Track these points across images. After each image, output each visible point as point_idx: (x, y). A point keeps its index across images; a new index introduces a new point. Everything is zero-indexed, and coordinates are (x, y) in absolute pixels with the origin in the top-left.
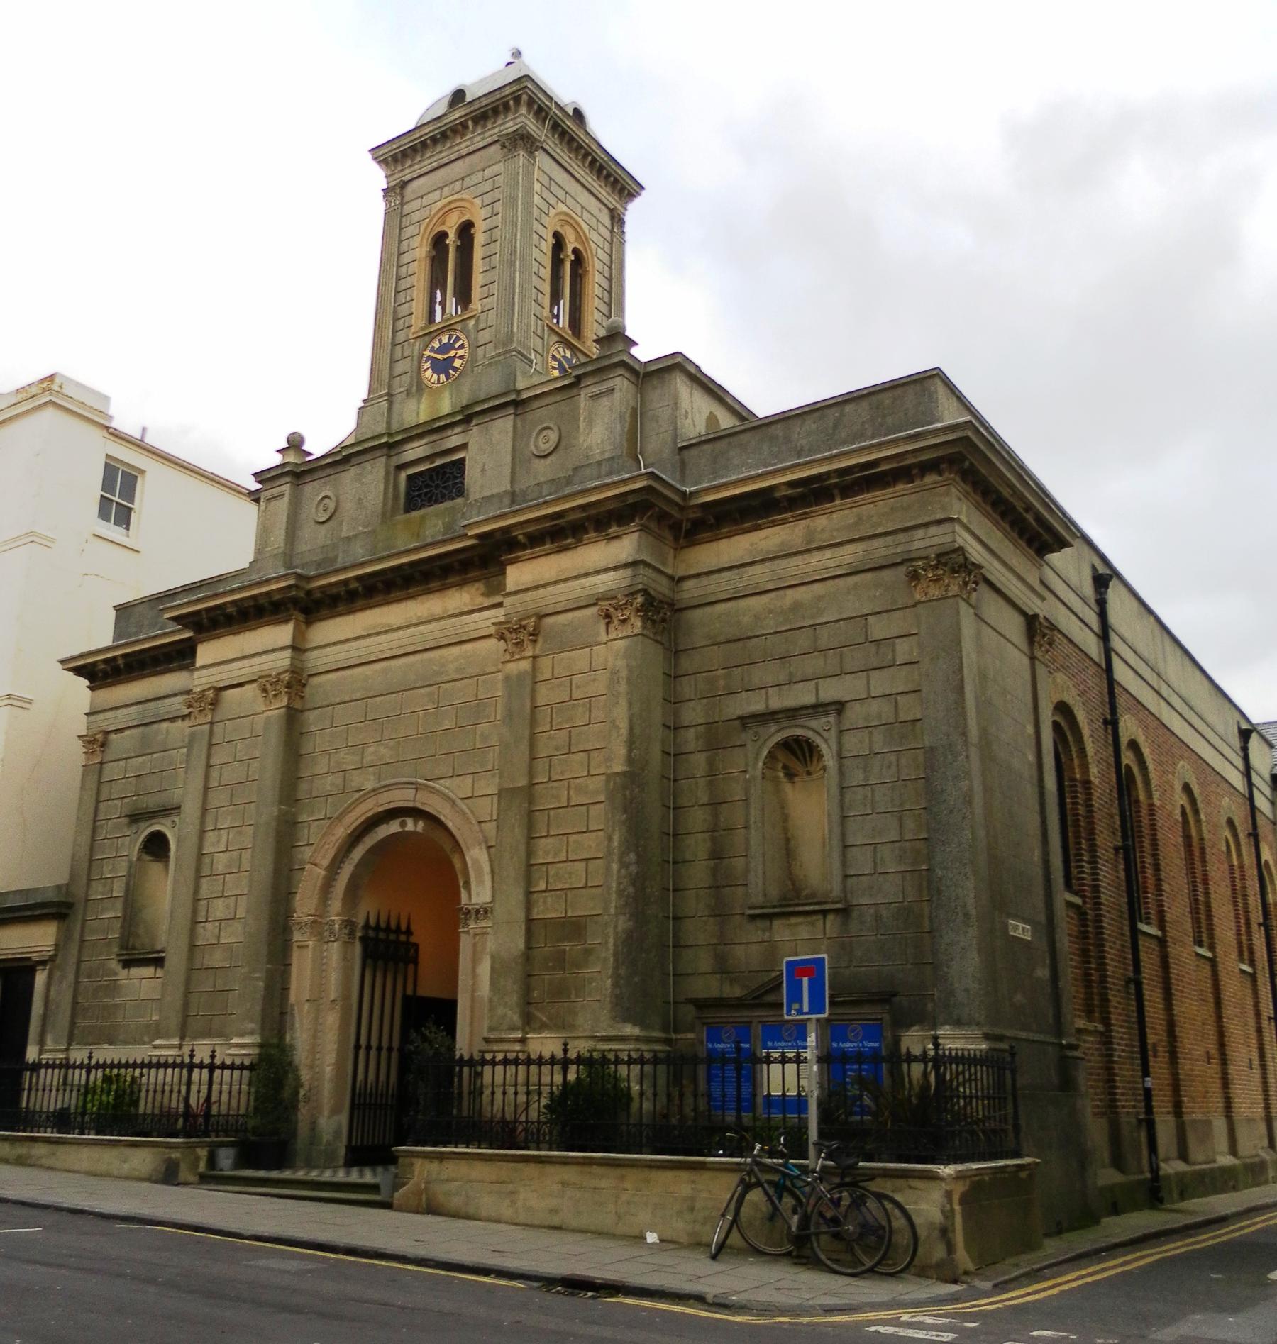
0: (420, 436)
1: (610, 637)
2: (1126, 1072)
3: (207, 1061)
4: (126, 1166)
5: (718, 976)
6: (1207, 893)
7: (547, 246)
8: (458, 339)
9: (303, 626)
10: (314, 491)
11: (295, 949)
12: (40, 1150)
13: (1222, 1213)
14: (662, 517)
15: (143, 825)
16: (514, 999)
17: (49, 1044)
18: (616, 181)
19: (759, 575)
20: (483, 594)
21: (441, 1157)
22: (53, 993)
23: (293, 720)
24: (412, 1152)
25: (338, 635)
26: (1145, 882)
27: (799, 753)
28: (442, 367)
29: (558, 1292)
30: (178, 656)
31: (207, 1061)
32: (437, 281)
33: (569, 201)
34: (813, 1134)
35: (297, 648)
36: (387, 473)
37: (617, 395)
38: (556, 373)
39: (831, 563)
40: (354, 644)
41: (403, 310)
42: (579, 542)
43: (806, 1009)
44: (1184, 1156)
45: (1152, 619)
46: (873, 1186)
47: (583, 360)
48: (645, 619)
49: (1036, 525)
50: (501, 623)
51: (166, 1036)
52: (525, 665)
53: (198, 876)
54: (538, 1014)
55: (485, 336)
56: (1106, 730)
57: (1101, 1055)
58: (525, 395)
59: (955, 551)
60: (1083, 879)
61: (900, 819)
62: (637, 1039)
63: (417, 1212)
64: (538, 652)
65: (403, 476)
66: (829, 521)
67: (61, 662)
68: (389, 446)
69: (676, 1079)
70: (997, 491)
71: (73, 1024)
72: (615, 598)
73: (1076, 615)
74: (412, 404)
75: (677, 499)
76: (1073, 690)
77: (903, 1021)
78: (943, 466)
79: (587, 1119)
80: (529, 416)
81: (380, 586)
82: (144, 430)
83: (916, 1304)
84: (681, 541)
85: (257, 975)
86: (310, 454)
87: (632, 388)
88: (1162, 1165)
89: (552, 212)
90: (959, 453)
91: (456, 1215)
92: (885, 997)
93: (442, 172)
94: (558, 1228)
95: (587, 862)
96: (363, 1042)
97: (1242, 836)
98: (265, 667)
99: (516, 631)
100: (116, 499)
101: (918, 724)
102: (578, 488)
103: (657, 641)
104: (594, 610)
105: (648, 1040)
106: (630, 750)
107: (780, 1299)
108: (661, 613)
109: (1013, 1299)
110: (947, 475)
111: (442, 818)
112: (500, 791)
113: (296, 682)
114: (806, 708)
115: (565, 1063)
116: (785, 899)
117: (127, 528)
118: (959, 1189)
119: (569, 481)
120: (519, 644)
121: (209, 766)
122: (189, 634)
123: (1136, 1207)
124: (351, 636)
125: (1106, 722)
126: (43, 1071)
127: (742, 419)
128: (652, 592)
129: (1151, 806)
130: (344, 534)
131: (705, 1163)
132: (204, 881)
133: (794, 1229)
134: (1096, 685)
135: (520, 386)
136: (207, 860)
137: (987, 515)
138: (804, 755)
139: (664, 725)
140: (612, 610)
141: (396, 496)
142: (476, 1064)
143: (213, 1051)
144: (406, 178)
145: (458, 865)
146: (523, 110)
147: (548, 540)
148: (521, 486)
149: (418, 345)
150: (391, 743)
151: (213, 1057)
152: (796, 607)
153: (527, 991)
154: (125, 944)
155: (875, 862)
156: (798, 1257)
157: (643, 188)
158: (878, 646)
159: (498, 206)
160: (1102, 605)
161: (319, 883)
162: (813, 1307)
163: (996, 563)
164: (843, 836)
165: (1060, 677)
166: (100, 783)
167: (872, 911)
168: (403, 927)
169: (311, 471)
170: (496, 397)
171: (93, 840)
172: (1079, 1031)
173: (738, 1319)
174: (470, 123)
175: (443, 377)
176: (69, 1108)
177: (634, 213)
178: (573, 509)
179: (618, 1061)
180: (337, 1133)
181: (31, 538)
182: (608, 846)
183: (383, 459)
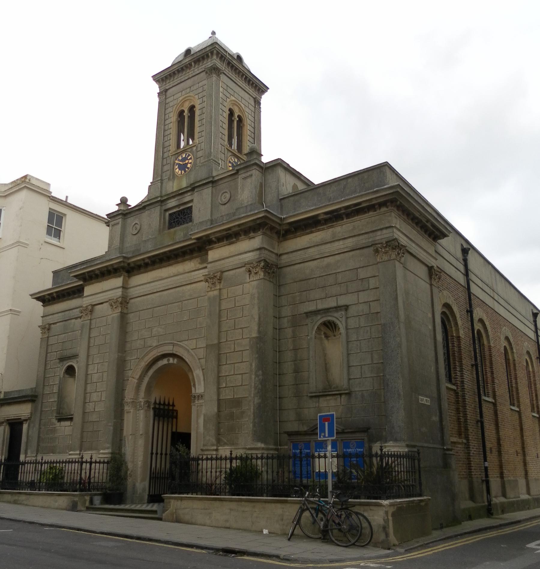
0: (174, 197)
1: (251, 280)
2: (476, 459)
3: (89, 460)
4: (57, 504)
5: (297, 422)
6: (516, 383)
7: (226, 114)
8: (189, 155)
9: (127, 278)
10: (131, 221)
11: (125, 413)
12: (23, 497)
13: (519, 519)
14: (272, 229)
15: (65, 362)
17: (29, 454)
18: (256, 86)
19: (313, 252)
20: (199, 263)
21: (182, 499)
22: (30, 433)
23: (123, 317)
24: (170, 497)
25: (142, 281)
26: (487, 379)
27: (330, 327)
28: (183, 167)
29: (220, 555)
30: (78, 292)
31: (89, 460)
32: (180, 131)
33: (236, 95)
34: (330, 488)
35: (125, 287)
36: (161, 213)
37: (254, 178)
38: (231, 168)
39: (342, 246)
40: (148, 285)
41: (167, 144)
42: (238, 240)
43: (327, 435)
44: (504, 495)
45: (490, 266)
46: (356, 509)
47: (242, 162)
48: (265, 272)
49: (433, 227)
50: (206, 275)
51: (74, 450)
53: (86, 384)
54: (223, 439)
55: (200, 154)
56: (468, 315)
57: (465, 453)
58: (216, 179)
59: (394, 240)
60: (457, 378)
61: (372, 354)
62: (263, 449)
63: (172, 521)
64: (221, 287)
65: (167, 214)
66: (342, 228)
67: (31, 295)
68: (162, 201)
69: (280, 465)
70: (413, 214)
71: (38, 445)
72: (252, 263)
73: (453, 266)
74: (171, 183)
75: (278, 221)
76: (452, 298)
77: (372, 440)
78: (388, 204)
79: (242, 482)
82: (67, 197)
83: (370, 558)
84: (281, 238)
85: (110, 424)
86: (130, 206)
87: (260, 174)
88: (494, 499)
89: (228, 100)
90: (395, 198)
91: (187, 523)
92: (366, 430)
93: (182, 84)
94: (229, 528)
95: (243, 375)
96: (154, 451)
97: (533, 359)
98: (111, 296)
99: (212, 278)
100: (54, 226)
101: (379, 314)
102: (237, 217)
103: (270, 281)
104: (244, 269)
105: (268, 449)
106: (259, 328)
107: (311, 556)
108: (272, 269)
109: (412, 556)
110: (390, 208)
111: (184, 357)
112: (207, 345)
114: (332, 308)
115: (231, 459)
117: (59, 239)
118: (391, 510)
119: (234, 214)
120: (214, 284)
121: (90, 338)
122: (81, 283)
123: (480, 517)
124: (146, 282)
125: (467, 311)
126: (26, 465)
127: (308, 185)
128: (268, 261)
129: (490, 347)
130: (144, 239)
131: (287, 500)
132: (88, 385)
133: (321, 527)
134: (463, 296)
135: (214, 174)
136: (89, 377)
137: (409, 224)
138: (332, 328)
139: (274, 317)
140: (251, 268)
141: (164, 222)
142: (197, 459)
143: (91, 456)
144: (167, 88)
145: (191, 377)
146: (215, 57)
147: (225, 240)
149: (173, 158)
150: (163, 326)
151: (91, 458)
154: (58, 413)
155: (361, 373)
156: (324, 539)
157: (268, 88)
158: (362, 281)
159: (205, 99)
160: (465, 261)
161: (135, 385)
162: (325, 560)
163: (414, 245)
164: (348, 361)
165: (445, 293)
166: (48, 345)
167: (360, 394)
168: (171, 403)
169: (130, 213)
170: (204, 179)
171: (45, 369)
172: (452, 442)
173: (292, 565)
174: (193, 63)
175: (183, 172)
176: (34, 480)
177: (265, 100)
178: (234, 226)
179: (252, 458)
180: (144, 490)
181: (18, 243)
183: (159, 207)
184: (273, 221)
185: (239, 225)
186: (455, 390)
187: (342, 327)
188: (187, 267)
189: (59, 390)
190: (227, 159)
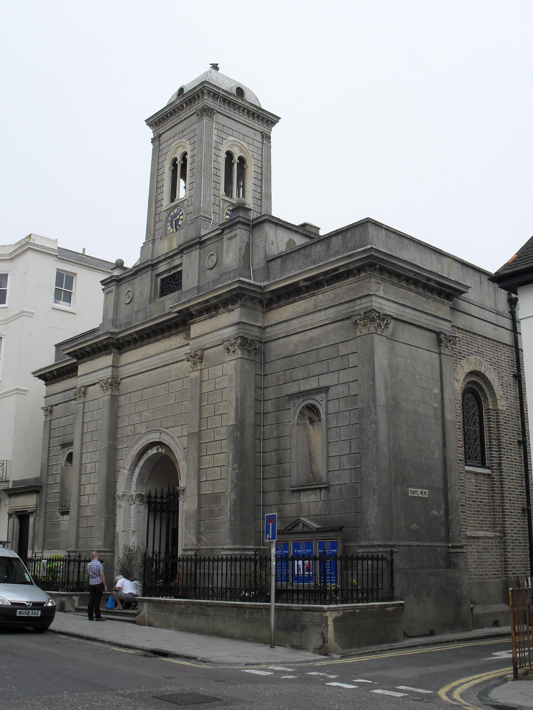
0: (164, 260)
8: (181, 210)
9: (118, 355)
10: (125, 287)
11: (118, 507)
14: (252, 299)
15: (66, 449)
16: (193, 531)
19: (296, 325)
22: (36, 527)
23: (114, 399)
35: (115, 366)
37: (238, 237)
40: (137, 364)
52: (197, 373)
64: (203, 367)
66: (324, 296)
67: (33, 373)
72: (230, 340)
78: (366, 269)
80: (206, 249)
81: (145, 336)
82: (84, 249)
85: (102, 520)
100: (63, 289)
104: (221, 347)
108: (253, 347)
112: (188, 434)
113: (114, 383)
116: (309, 482)
121: (83, 423)
122: (76, 360)
136: (83, 466)
140: (229, 346)
141: (156, 289)
144: (160, 133)
148: (201, 284)
150: (151, 411)
151: (80, 557)
152: (311, 339)
153: (199, 527)
157: (280, 118)
164: (327, 451)
174: (184, 105)
177: (276, 132)
178: (212, 298)
182: (228, 460)
184: (252, 291)
185: (216, 297)
186: (489, 475)
187: (322, 410)
188: (170, 347)
189: (61, 480)
190: (223, 210)
